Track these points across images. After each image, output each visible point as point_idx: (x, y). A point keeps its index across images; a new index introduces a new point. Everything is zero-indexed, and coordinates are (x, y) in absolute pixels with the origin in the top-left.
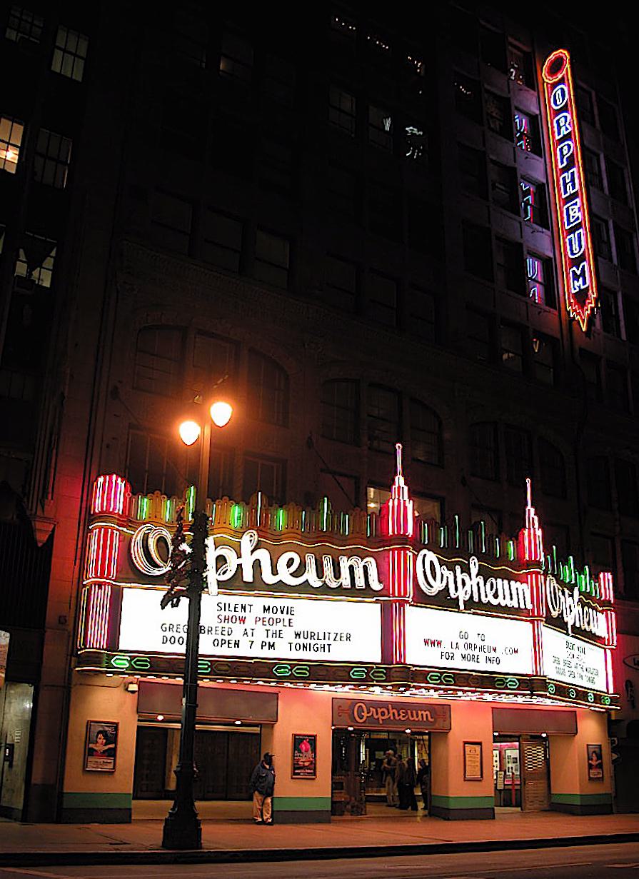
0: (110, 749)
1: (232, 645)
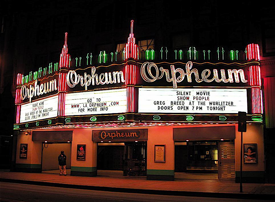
0: (253, 154)
1: (186, 109)
